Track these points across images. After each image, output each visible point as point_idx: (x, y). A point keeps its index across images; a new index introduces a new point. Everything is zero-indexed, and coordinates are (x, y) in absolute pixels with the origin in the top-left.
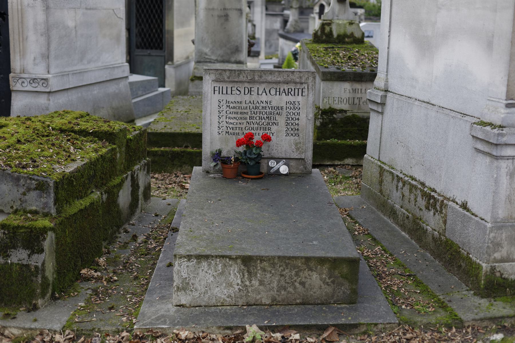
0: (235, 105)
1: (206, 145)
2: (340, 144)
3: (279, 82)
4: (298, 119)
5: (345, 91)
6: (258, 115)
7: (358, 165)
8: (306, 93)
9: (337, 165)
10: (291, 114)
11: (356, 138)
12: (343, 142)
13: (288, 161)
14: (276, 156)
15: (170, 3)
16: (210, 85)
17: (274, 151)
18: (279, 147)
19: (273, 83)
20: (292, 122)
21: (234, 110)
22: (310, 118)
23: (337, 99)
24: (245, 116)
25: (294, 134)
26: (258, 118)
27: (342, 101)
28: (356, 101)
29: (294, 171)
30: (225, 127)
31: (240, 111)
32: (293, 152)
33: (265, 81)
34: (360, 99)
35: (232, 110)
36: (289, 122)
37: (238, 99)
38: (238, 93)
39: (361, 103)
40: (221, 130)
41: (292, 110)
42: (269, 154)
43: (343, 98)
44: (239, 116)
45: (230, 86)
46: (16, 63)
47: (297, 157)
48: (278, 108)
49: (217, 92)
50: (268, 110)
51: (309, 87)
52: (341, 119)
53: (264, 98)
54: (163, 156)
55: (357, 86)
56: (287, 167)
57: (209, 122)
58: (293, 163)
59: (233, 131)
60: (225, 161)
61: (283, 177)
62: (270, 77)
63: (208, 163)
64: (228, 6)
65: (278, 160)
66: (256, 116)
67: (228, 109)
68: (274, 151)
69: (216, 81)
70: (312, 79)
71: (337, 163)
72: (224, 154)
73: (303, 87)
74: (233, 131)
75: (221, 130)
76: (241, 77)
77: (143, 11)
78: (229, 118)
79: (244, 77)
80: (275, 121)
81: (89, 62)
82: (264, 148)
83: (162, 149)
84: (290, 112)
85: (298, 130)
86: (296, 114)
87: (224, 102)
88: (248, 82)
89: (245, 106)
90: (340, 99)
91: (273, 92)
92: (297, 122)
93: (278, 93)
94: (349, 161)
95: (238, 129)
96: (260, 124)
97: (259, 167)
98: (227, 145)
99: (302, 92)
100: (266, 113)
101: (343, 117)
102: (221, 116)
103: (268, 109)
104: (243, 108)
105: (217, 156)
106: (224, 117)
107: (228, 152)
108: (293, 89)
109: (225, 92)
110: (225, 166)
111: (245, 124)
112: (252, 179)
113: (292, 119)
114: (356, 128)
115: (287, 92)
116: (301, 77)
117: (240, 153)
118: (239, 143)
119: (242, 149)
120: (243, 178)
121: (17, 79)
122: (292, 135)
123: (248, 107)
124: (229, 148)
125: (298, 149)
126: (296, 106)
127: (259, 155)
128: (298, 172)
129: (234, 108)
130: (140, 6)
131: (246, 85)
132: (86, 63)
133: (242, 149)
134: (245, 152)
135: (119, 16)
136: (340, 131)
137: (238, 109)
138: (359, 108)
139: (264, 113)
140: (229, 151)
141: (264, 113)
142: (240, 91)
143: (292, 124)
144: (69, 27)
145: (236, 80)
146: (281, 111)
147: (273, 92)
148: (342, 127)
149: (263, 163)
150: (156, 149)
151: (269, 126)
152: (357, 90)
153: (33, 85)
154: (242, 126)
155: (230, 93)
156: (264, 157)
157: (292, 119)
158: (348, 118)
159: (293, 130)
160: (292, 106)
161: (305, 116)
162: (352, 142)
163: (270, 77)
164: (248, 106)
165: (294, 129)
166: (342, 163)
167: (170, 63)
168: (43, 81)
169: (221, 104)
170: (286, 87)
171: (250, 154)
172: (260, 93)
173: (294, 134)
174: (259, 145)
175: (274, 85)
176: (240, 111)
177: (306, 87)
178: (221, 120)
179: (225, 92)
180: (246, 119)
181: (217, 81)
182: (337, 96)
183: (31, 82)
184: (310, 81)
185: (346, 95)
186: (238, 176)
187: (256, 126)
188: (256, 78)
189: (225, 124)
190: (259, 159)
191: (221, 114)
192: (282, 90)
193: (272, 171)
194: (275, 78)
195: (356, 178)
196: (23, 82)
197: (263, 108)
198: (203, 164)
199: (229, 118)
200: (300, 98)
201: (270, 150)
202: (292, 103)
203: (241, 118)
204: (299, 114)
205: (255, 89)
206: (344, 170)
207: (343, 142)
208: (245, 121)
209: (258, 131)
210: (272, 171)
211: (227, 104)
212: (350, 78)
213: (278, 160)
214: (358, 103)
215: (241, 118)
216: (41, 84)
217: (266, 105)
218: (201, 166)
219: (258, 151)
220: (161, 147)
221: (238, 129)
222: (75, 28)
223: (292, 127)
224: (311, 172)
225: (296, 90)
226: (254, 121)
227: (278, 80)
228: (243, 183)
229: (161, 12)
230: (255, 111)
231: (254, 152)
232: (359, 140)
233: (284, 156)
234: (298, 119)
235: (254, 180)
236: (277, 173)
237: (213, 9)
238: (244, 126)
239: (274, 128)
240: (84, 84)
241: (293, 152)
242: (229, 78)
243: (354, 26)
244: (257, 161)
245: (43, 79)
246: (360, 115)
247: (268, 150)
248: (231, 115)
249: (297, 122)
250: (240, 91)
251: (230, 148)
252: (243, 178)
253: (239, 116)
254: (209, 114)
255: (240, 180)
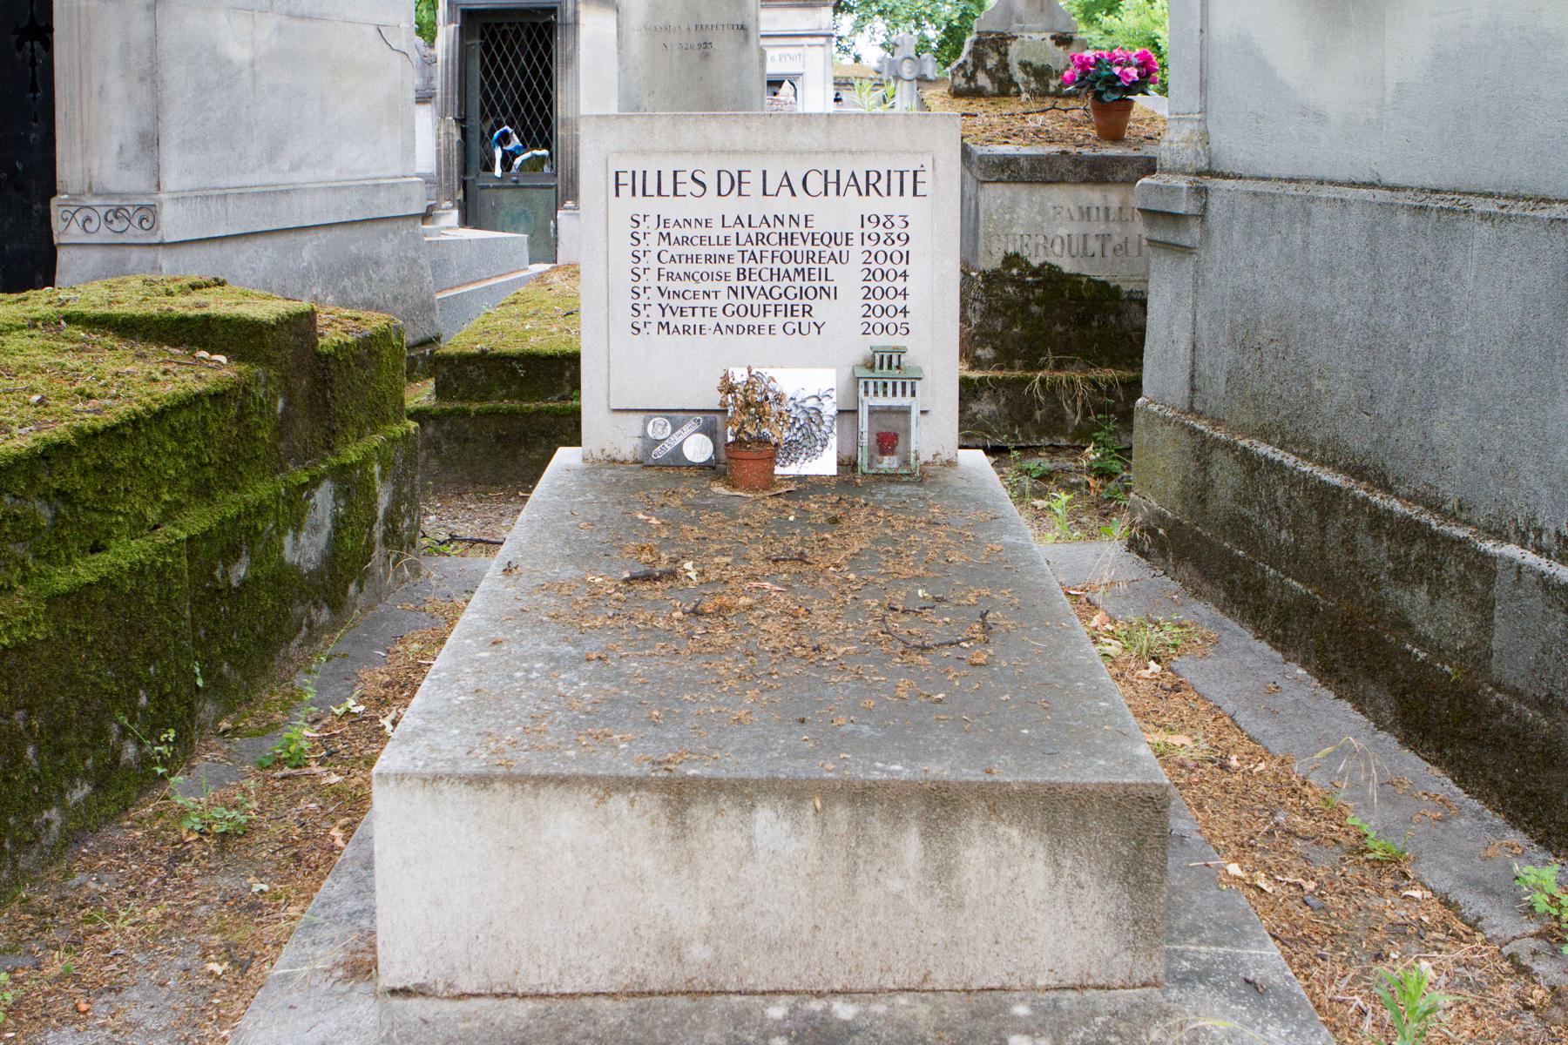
6: (767, 262)
10: (881, 257)
15: (570, 48)
24: (723, 267)
25: (892, 329)
35: (677, 250)
36: (872, 285)
38: (699, 190)
41: (881, 246)
43: (1050, 238)
46: (69, 168)
48: (833, 238)
50: (800, 247)
64: (707, 19)
66: (759, 267)
67: (664, 245)
77: (499, 73)
78: (670, 276)
81: (295, 167)
86: (896, 257)
87: (652, 221)
89: (723, 233)
93: (832, 188)
96: (776, 293)
103: (800, 241)
104: (714, 241)
106: (653, 274)
111: (723, 296)
121: (73, 210)
126: (896, 231)
130: (493, 60)
132: (286, 167)
139: (786, 257)
141: (786, 257)
144: (230, 62)
146: (843, 248)
151: (805, 301)
153: (117, 226)
155: (671, 192)
157: (884, 275)
160: (880, 230)
164: (731, 232)
167: (569, 204)
168: (143, 213)
169: (642, 229)
173: (892, 329)
178: (641, 284)
183: (110, 216)
187: (762, 300)
189: (655, 297)
191: (642, 265)
196: (88, 219)
199: (670, 276)
202: (883, 220)
203: (710, 276)
215: (710, 276)
216: (136, 221)
218: (579, 444)
221: (698, 312)
222: (252, 65)
229: (548, 72)
237: (667, 28)
240: (275, 227)
245: (141, 207)
250: (703, 185)
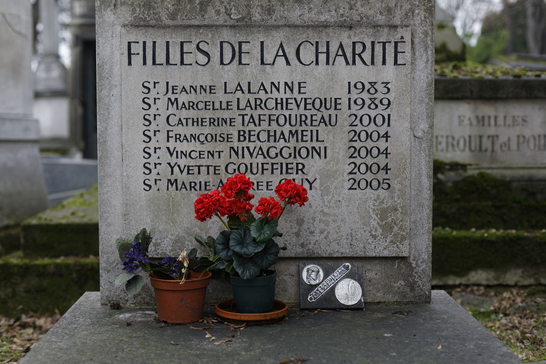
0: (193, 97)
1: (109, 225)
2: (457, 239)
3: (325, 26)
4: (386, 136)
5: (461, 122)
6: (265, 125)
7: (501, 286)
8: (408, 55)
9: (454, 287)
10: (366, 120)
11: (488, 225)
12: (463, 233)
13: (358, 264)
14: (324, 250)
16: (116, 41)
17: (317, 237)
18: (332, 225)
19: (308, 27)
20: (369, 144)
21: (192, 114)
22: (420, 134)
23: (444, 140)
24: (225, 129)
25: (375, 184)
26: (264, 136)
27: (455, 143)
28: (486, 143)
29: (379, 296)
30: (164, 165)
31: (208, 115)
32: (375, 237)
33: (282, 22)
34: (493, 138)
35: (184, 114)
36: (358, 145)
37: (204, 78)
38: (203, 59)
39: (497, 148)
40: (153, 176)
41: (366, 110)
42: (302, 245)
43: (457, 138)
44: (207, 130)
45: (175, 39)
47: (386, 253)
48: (323, 102)
49: (137, 60)
50: (294, 111)
51: (416, 40)
52: (456, 183)
53: (281, 73)
54: (61, 275)
55: (487, 110)
56: (357, 284)
57: (117, 154)
58: (373, 272)
59: (191, 178)
60: (163, 269)
61: (347, 316)
62: (298, 12)
63: (114, 279)
65: (329, 262)
66: (258, 129)
67: (172, 110)
68: (317, 237)
69: (138, 25)
70: (422, 14)
71: (452, 280)
72: (162, 247)
73: (397, 38)
74: (191, 178)
75: (153, 176)
76: (211, 12)
78: (178, 138)
79: (218, 12)
80: (315, 144)
82: (284, 224)
83: (59, 261)
84: (360, 113)
85: (386, 169)
86: (379, 120)
87: (162, 88)
88: (232, 27)
89: (225, 98)
90: (450, 140)
91: (308, 54)
92: (382, 144)
93: (322, 57)
94: (480, 276)
95: (204, 170)
96: (273, 153)
97: (270, 286)
98: (174, 221)
99: (396, 53)
100: (288, 119)
101: (458, 178)
102: (151, 134)
103: (294, 106)
104: (217, 106)
105: (136, 252)
106: (162, 136)
107: (176, 241)
108: (369, 46)
109: (161, 58)
110: (164, 284)
112: (249, 324)
113: (369, 136)
114: (490, 203)
115: (349, 55)
116: (389, 10)
117: (210, 243)
118: (204, 209)
119: (216, 226)
120: (222, 320)
122: (369, 184)
123: (235, 104)
124: (179, 231)
125: (387, 228)
126: (379, 96)
127: (270, 246)
128: (390, 298)
129: (192, 105)
131: (226, 35)
133: (216, 226)
134: (226, 237)
135: (17, 28)
136: (453, 210)
137: (202, 110)
138: (493, 159)
139: (282, 121)
140: (178, 242)
141: (282, 121)
142: (206, 54)
143: (369, 152)
145: (196, 23)
146: (332, 112)
147: (308, 54)
148: (457, 200)
149: (285, 273)
150: (46, 261)
152: (486, 120)
154: (215, 161)
156: (286, 254)
157: (369, 136)
158: (470, 181)
159: (372, 169)
160: (365, 96)
161: (407, 125)
162: (485, 234)
163: (298, 12)
164: (233, 98)
165: (375, 168)
166: (463, 280)
169: (153, 94)
170: (346, 39)
171: (241, 243)
172: (269, 58)
173: (375, 184)
174: (271, 212)
175: (310, 32)
176: (208, 115)
177: (408, 38)
179: (161, 58)
180: (228, 138)
181: (138, 26)
182: (444, 133)
184: (417, 20)
185: (463, 131)
186: (204, 315)
187: (261, 159)
188: (257, 17)
190: (271, 258)
191: (153, 127)
192: (334, 48)
193: (311, 297)
194: (313, 15)
195: (506, 315)
197: (280, 104)
198: (102, 282)
199: (178, 138)
200: (389, 72)
201: (303, 233)
202: (367, 86)
203: (214, 138)
204: (387, 120)
205: (252, 48)
206: (471, 296)
207: (463, 233)
208: (224, 147)
209: (267, 176)
210: (311, 297)
211: (170, 95)
212: (472, 91)
213: (330, 263)
214: (490, 149)
215: (214, 138)
217: (288, 95)
219: (267, 232)
220: (57, 256)
221: (204, 170)
223: (369, 161)
224: (429, 297)
225: (378, 48)
226: (252, 146)
227: (322, 18)
228: (219, 338)
230: (255, 114)
231: (254, 234)
232: (497, 229)
233: (347, 251)
234: (386, 136)
235: (255, 329)
236: (330, 305)
238: (221, 162)
239: (314, 166)
241: (375, 237)
242: (173, 16)
243: (446, 32)
244: (264, 264)
246: (496, 173)
247: (298, 234)
248: (181, 130)
249: (382, 144)
250: (206, 54)
251: (179, 232)
252: (222, 320)
253: (207, 130)
254: (117, 129)
255: (209, 329)
